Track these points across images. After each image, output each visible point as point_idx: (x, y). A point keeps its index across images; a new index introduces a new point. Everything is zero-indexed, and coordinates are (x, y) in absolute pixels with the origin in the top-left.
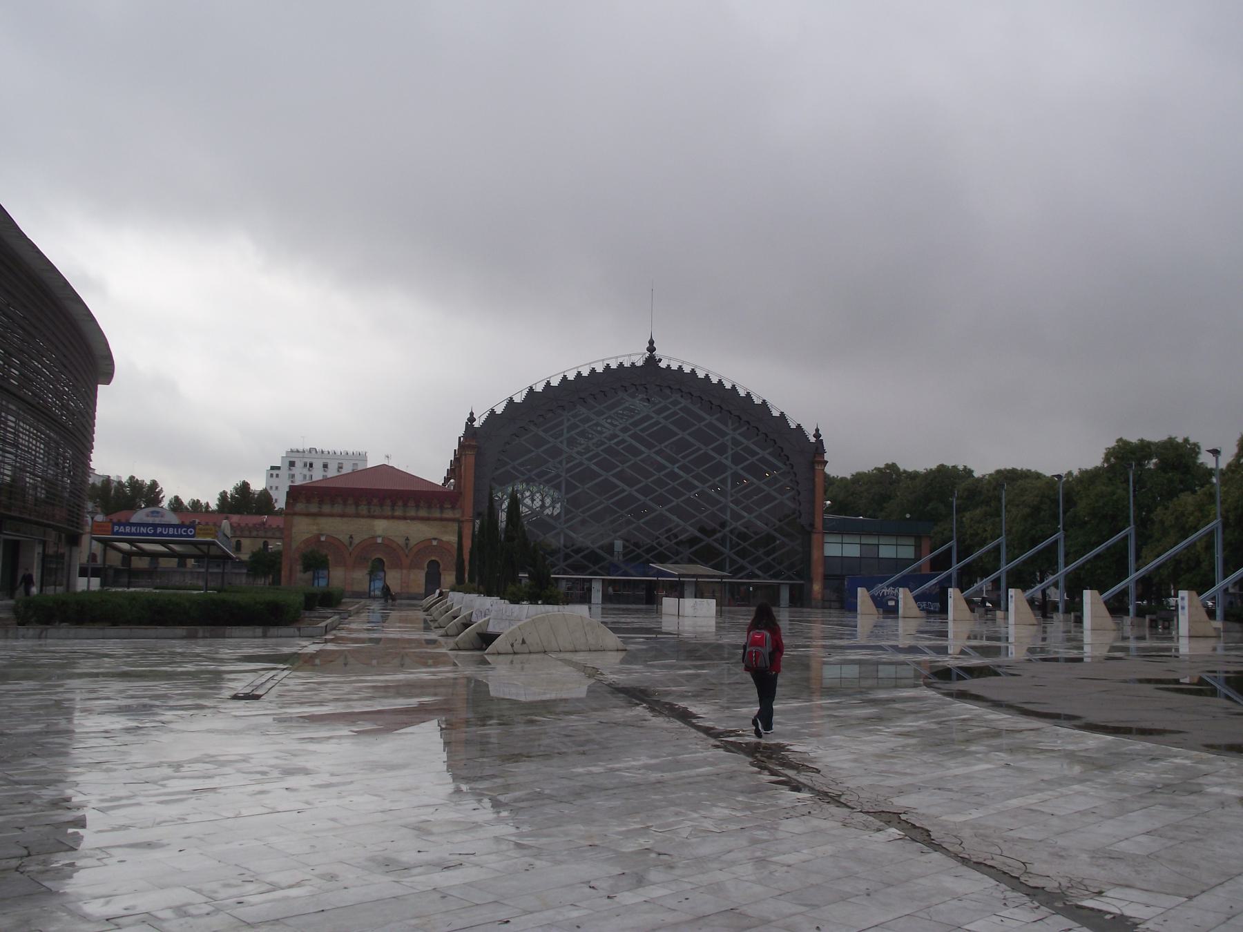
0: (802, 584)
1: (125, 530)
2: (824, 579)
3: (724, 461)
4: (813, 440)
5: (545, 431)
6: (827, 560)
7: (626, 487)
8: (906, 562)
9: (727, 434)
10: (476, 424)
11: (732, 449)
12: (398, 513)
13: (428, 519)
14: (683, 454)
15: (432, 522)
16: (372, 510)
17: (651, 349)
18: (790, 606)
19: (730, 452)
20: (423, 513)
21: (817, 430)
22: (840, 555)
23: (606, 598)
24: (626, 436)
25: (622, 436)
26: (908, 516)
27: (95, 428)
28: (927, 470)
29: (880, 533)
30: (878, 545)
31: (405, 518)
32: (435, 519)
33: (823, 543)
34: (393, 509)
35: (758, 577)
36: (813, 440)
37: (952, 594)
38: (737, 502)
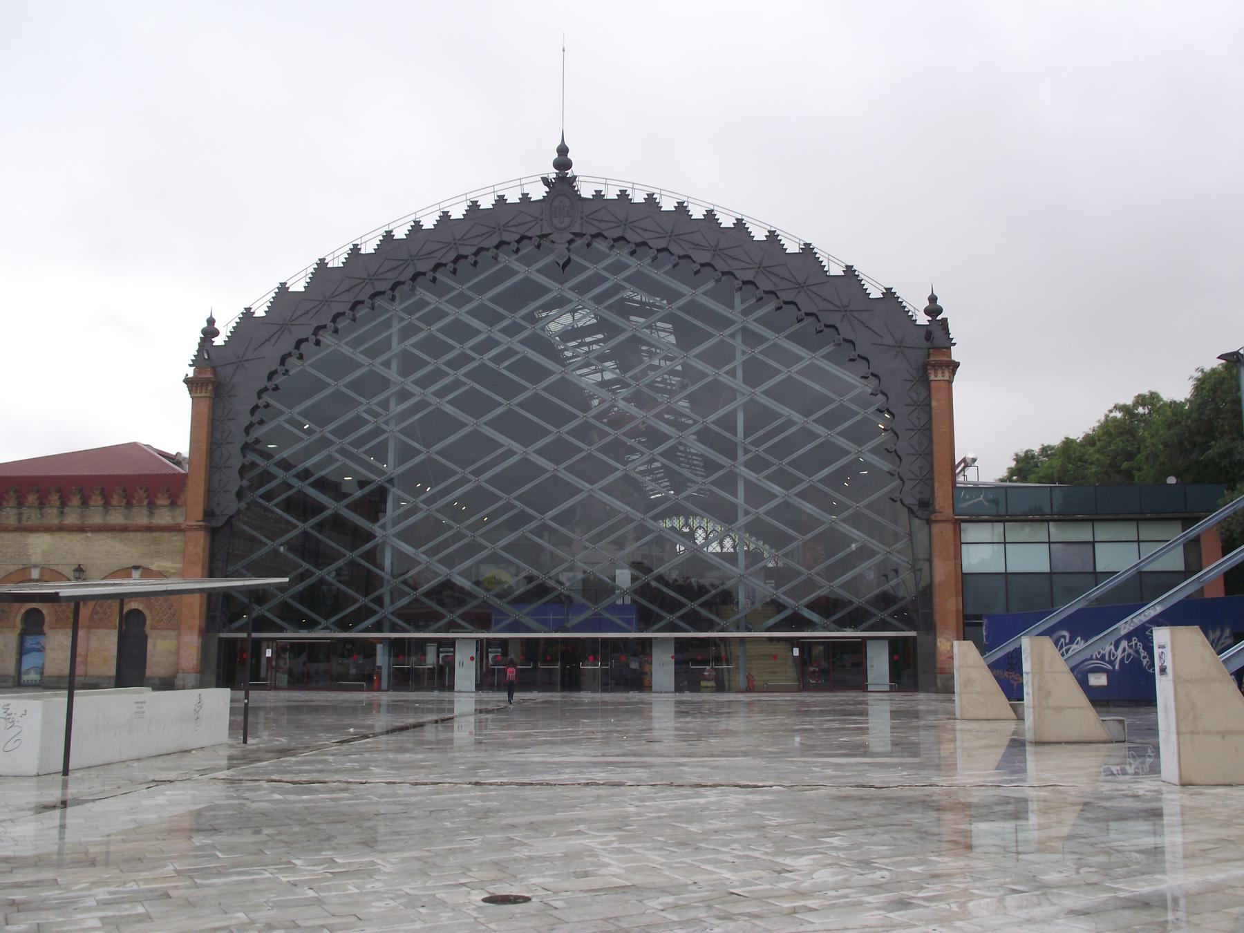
0: (914, 638)
1: (722, 548)
2: (965, 625)
3: (726, 379)
4: (923, 319)
5: (354, 344)
6: (966, 581)
7: (515, 446)
8: (1167, 580)
9: (732, 322)
10: (219, 341)
11: (744, 353)
12: (72, 519)
13: (124, 529)
14: (593, 532)
15: (131, 535)
16: (24, 517)
17: (563, 162)
18: (678, 689)
19: (740, 359)
20: (116, 517)
21: (933, 299)
22: (1004, 571)
23: (484, 682)
24: (515, 343)
25: (506, 342)
26: (1171, 480)
27: (1077, 434)
28: (1202, 371)
29: (1094, 517)
30: (1093, 543)
31: (82, 529)
32: (138, 529)
33: (958, 544)
34: (62, 513)
35: (809, 625)
36: (923, 319)
37: (1168, 651)
38: (756, 464)
